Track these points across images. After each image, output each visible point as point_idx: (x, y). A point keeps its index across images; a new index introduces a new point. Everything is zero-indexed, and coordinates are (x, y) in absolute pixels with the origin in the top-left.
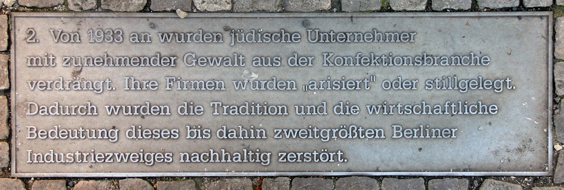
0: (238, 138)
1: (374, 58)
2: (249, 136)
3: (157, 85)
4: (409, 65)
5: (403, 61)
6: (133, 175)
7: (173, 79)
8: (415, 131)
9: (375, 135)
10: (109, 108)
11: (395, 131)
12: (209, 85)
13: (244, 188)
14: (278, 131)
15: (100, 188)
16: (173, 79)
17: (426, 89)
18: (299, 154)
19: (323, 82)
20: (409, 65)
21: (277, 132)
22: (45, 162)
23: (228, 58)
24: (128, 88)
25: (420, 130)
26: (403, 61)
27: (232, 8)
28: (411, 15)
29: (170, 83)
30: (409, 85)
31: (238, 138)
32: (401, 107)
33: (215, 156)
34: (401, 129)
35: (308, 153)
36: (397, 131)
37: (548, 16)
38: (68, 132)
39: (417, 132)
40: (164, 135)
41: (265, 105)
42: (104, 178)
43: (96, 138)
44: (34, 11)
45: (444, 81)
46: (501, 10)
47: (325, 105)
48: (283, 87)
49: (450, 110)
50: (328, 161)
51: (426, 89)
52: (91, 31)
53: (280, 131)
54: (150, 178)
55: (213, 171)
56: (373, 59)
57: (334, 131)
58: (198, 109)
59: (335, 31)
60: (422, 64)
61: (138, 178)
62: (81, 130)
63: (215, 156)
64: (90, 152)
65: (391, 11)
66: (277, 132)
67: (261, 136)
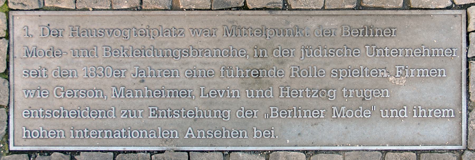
0: (446, 117)
1: (123, 51)
2: (217, 115)
3: (213, 73)
4: (427, 56)
5: (198, 53)
6: (402, 148)
7: (402, 68)
8: (361, 30)
9: (30, 115)
10: (26, 92)
11: (272, 112)
12: (210, 73)
13: (16, 159)
14: (124, 112)
15: (292, 158)
16: (402, 68)
17: (332, 77)
18: (100, 132)
19: (249, 70)
20: (427, 56)
21: (123, 112)
22: (32, 138)
23: (208, 50)
24: (160, 76)
25: (294, 111)
26: (198, 53)
27: (76, 8)
28: (305, 13)
29: (399, 71)
30: (376, 73)
31: (446, 117)
32: (125, 132)
33: (226, 133)
34: (277, 110)
35: (210, 131)
36: (274, 112)
37: (461, 15)
38: (77, 112)
39: (291, 112)
40: (247, 115)
41: (129, 130)
42: (396, 150)
43: (136, 117)
44: (237, 10)
45: (406, 70)
46: (434, 9)
47: (271, 89)
48: (434, 74)
49: (304, 95)
50: (38, 137)
51: (332, 77)
52: (26, 27)
53: (126, 111)
54: (416, 150)
55: (103, 146)
56: (122, 51)
57: (430, 111)
58: (44, 92)
59: (253, 27)
60: (189, 56)
61: (375, 150)
62: (41, 111)
63: (226, 133)
64: (127, 129)
65: (247, 9)
66: (123, 112)
67: (102, 115)
